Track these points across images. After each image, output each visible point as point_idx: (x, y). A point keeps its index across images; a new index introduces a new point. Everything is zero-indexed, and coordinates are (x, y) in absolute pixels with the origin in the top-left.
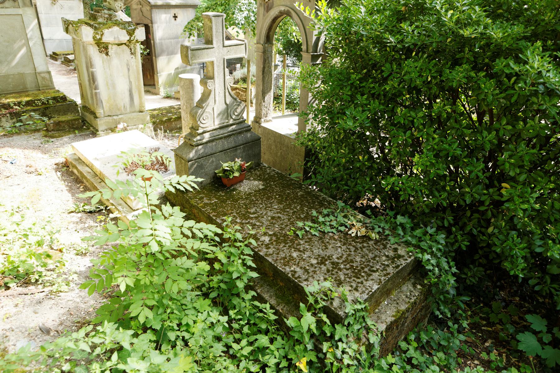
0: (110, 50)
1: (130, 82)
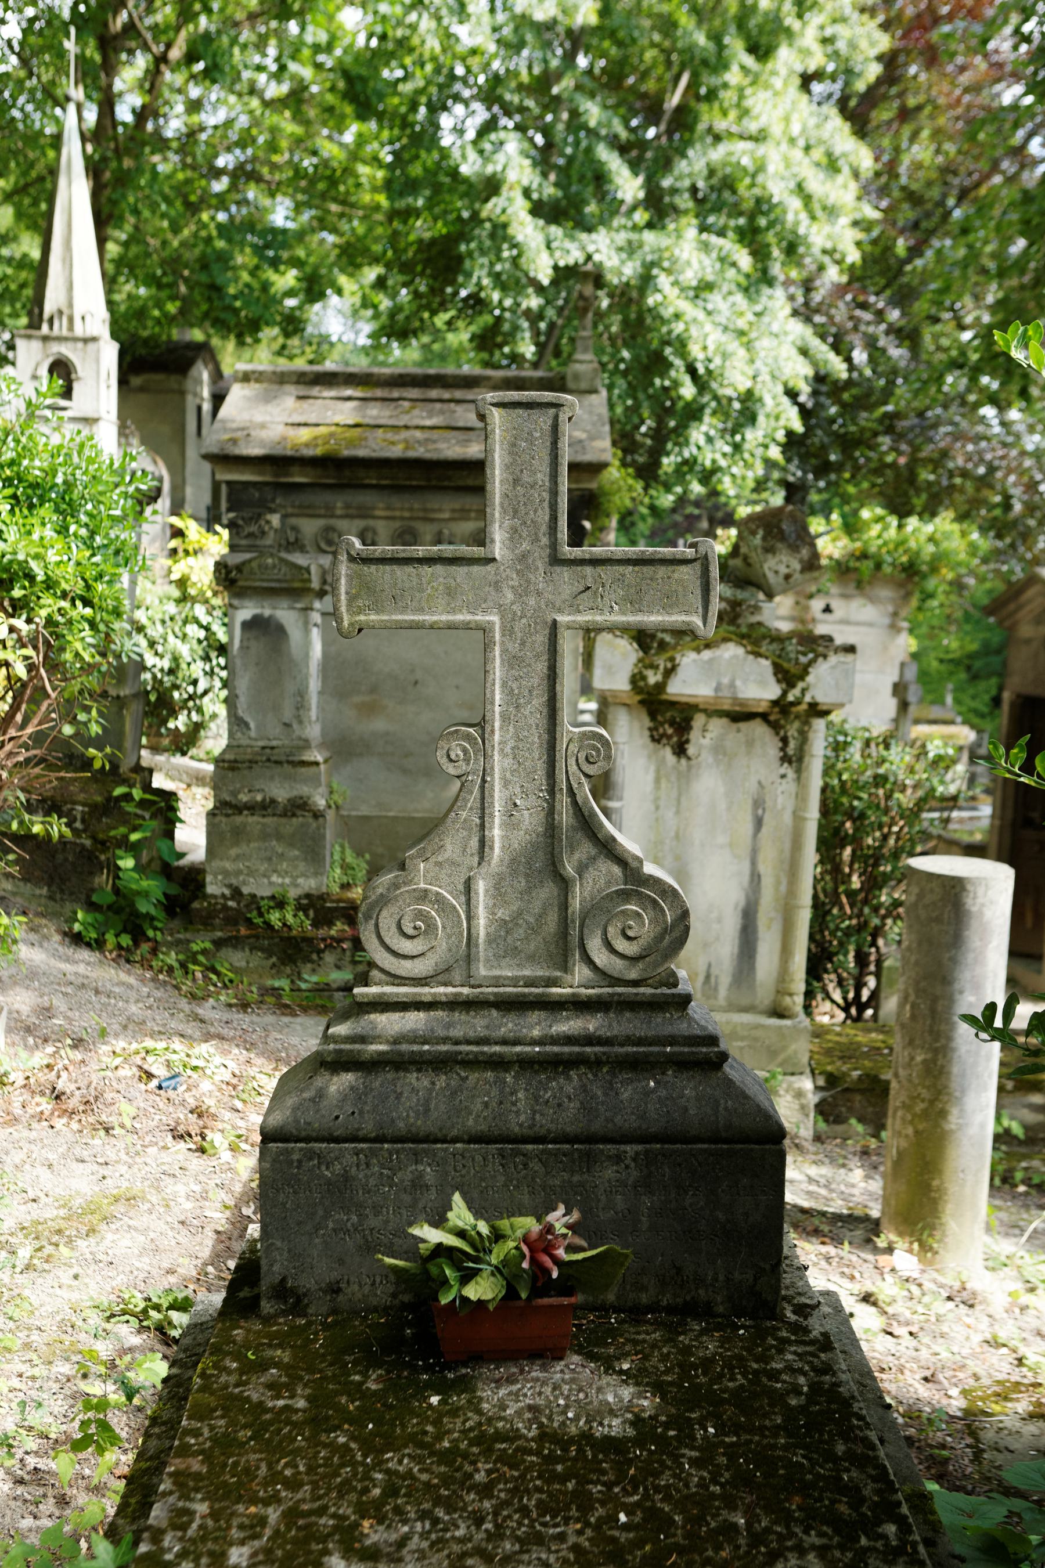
0: (694, 735)
1: (755, 878)
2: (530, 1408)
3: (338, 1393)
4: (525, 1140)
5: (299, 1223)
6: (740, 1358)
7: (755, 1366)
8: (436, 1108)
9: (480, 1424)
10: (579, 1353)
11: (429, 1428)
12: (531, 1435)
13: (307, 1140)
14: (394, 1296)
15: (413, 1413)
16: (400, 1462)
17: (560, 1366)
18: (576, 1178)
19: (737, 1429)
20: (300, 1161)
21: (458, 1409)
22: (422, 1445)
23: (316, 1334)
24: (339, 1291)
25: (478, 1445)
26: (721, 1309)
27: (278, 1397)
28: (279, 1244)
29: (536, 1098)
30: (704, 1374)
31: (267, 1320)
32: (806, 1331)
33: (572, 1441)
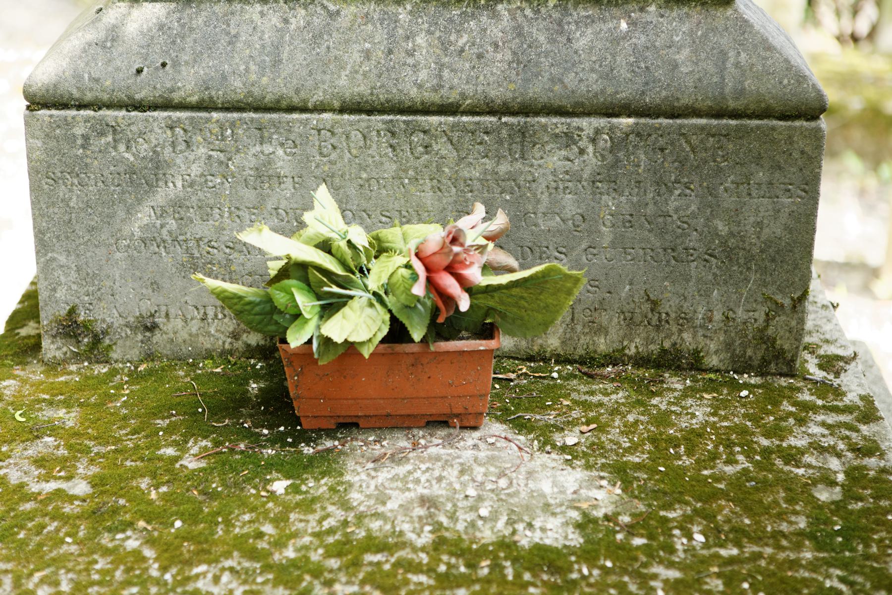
2: (424, 501)
3: (137, 473)
4: (426, 111)
5: (91, 230)
6: (743, 431)
7: (765, 442)
8: (291, 59)
9: (345, 523)
10: (502, 420)
11: (268, 529)
12: (420, 542)
13: (96, 105)
14: (235, 336)
15: (244, 505)
16: (216, 580)
17: (471, 438)
18: (504, 168)
19: (739, 535)
20: (86, 138)
21: (314, 500)
22: (253, 554)
23: (119, 387)
24: (152, 328)
25: (339, 555)
26: (713, 361)
27: (48, 478)
28: (62, 259)
29: (445, 45)
30: (690, 453)
31: (53, 367)
32: (838, 393)
33: (483, 552)
